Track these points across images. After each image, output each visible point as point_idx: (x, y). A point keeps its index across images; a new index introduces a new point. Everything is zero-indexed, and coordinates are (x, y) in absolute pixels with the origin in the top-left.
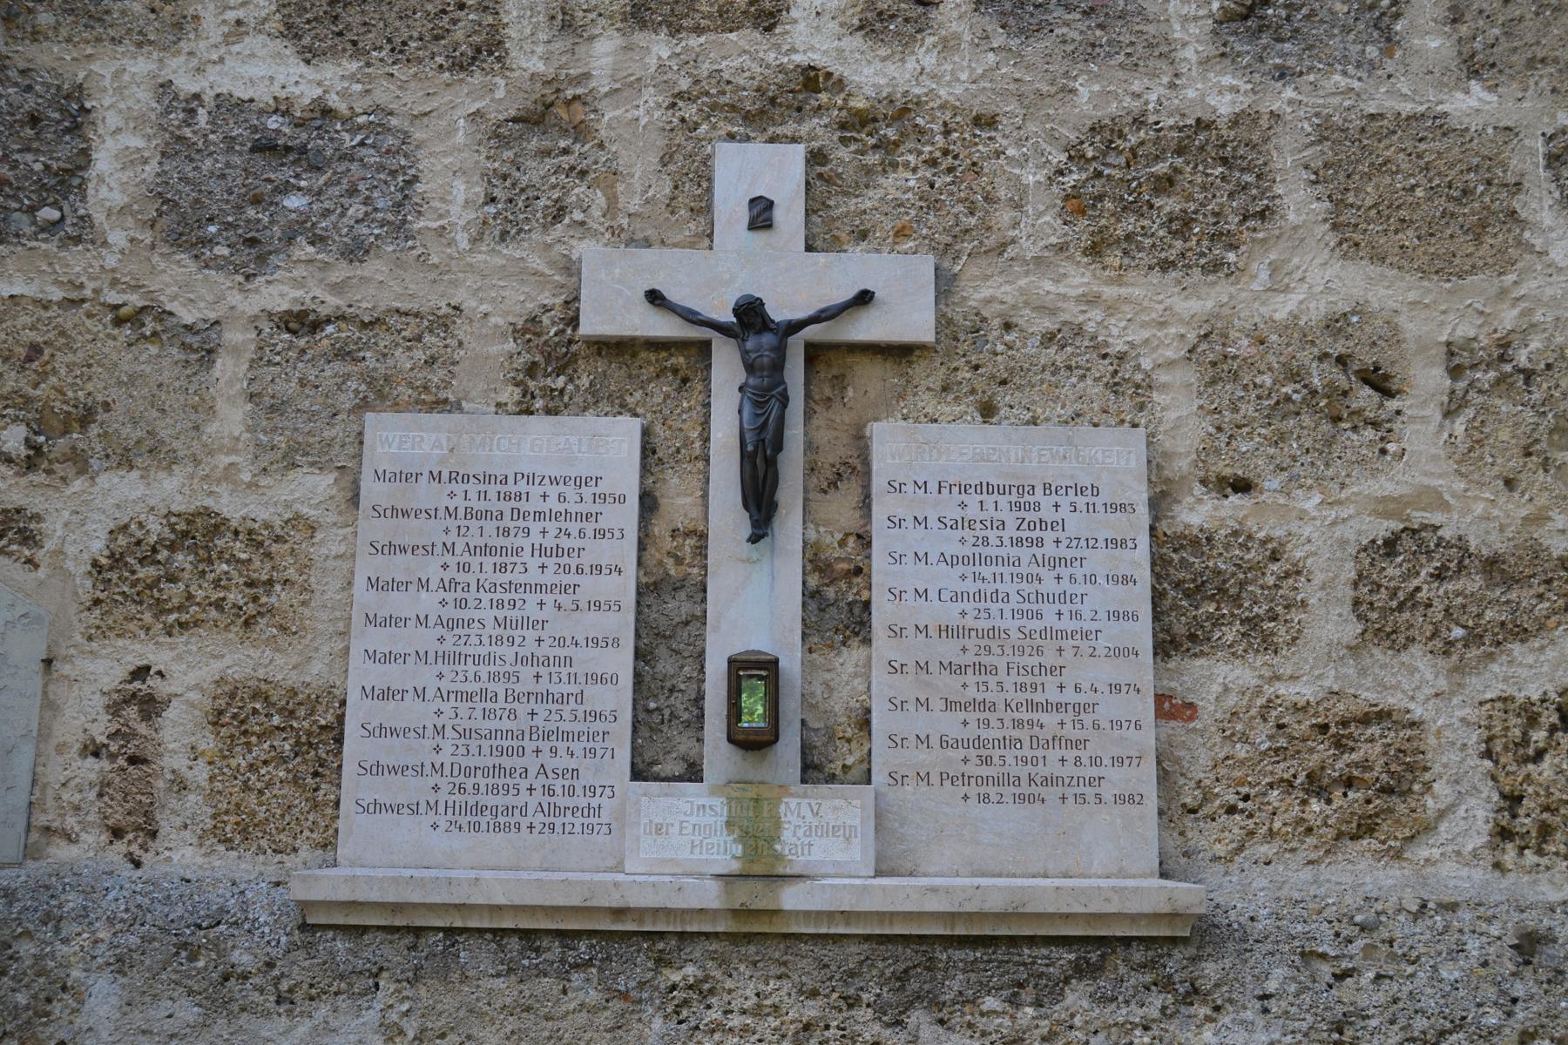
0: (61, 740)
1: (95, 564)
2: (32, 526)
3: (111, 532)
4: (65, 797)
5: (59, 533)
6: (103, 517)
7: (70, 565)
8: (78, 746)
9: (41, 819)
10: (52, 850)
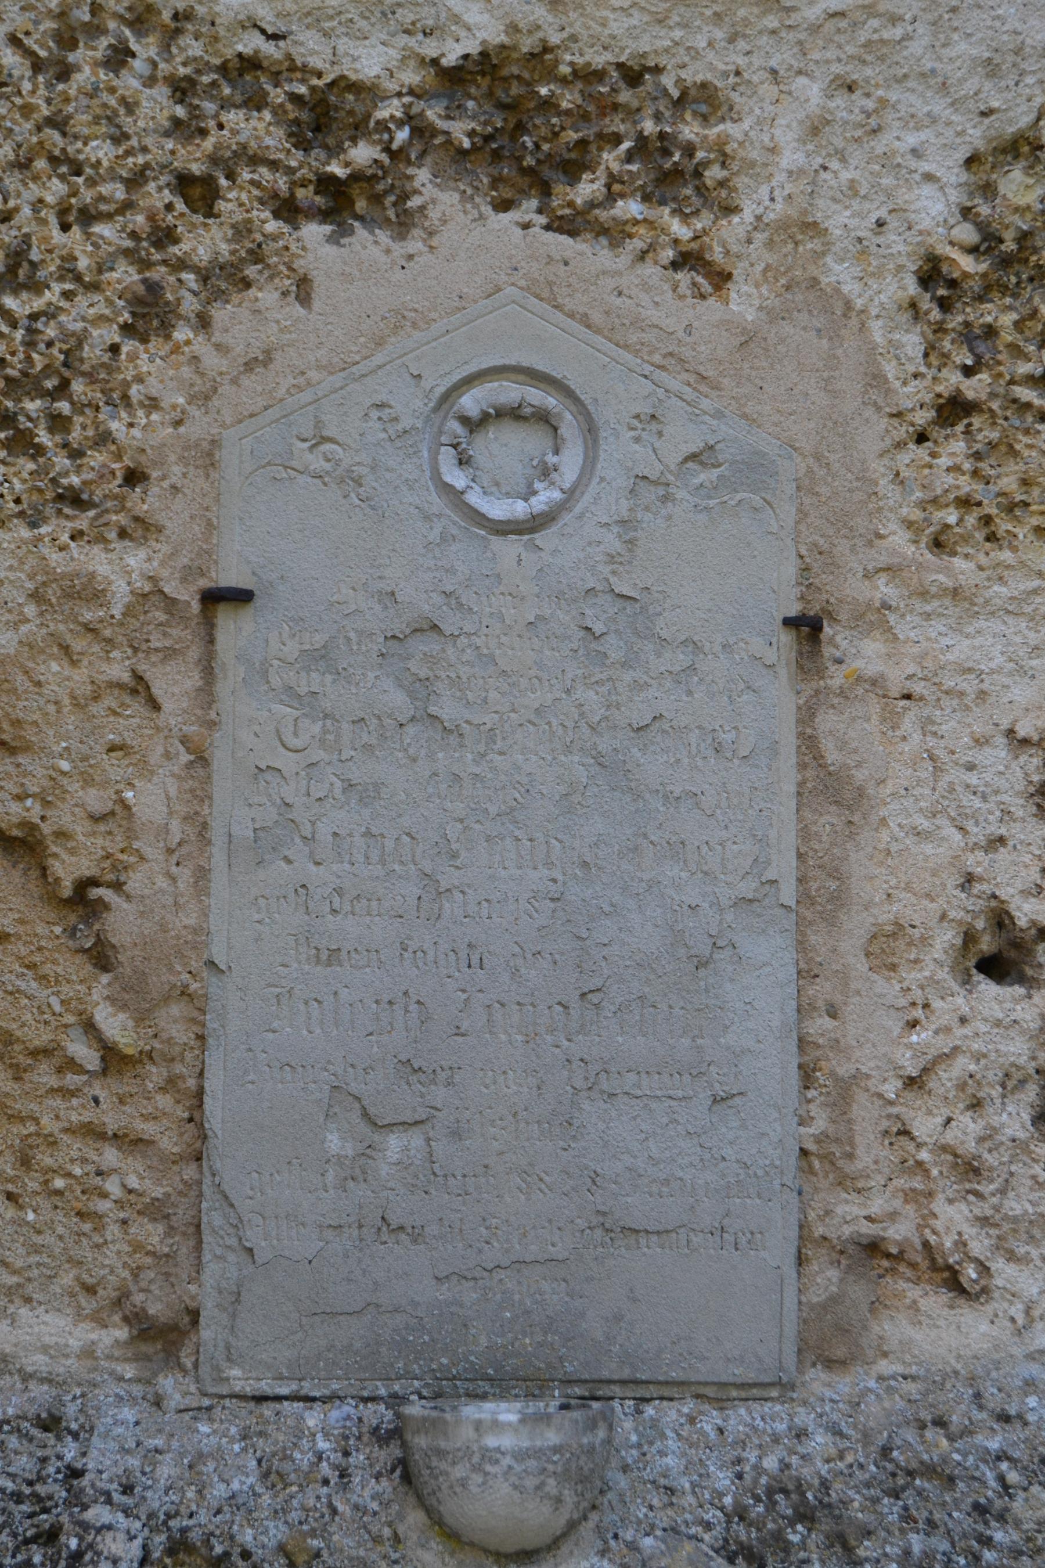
0: (885, 915)
1: (931, 272)
2: (689, 131)
3: (972, 161)
4: (925, 1126)
5: (791, 157)
6: (939, 106)
7: (841, 274)
8: (947, 938)
9: (849, 1215)
10: (893, 1328)
